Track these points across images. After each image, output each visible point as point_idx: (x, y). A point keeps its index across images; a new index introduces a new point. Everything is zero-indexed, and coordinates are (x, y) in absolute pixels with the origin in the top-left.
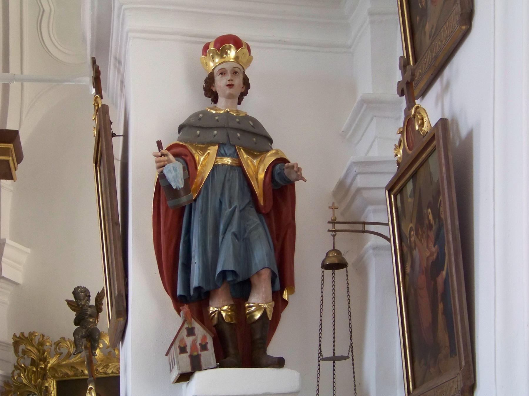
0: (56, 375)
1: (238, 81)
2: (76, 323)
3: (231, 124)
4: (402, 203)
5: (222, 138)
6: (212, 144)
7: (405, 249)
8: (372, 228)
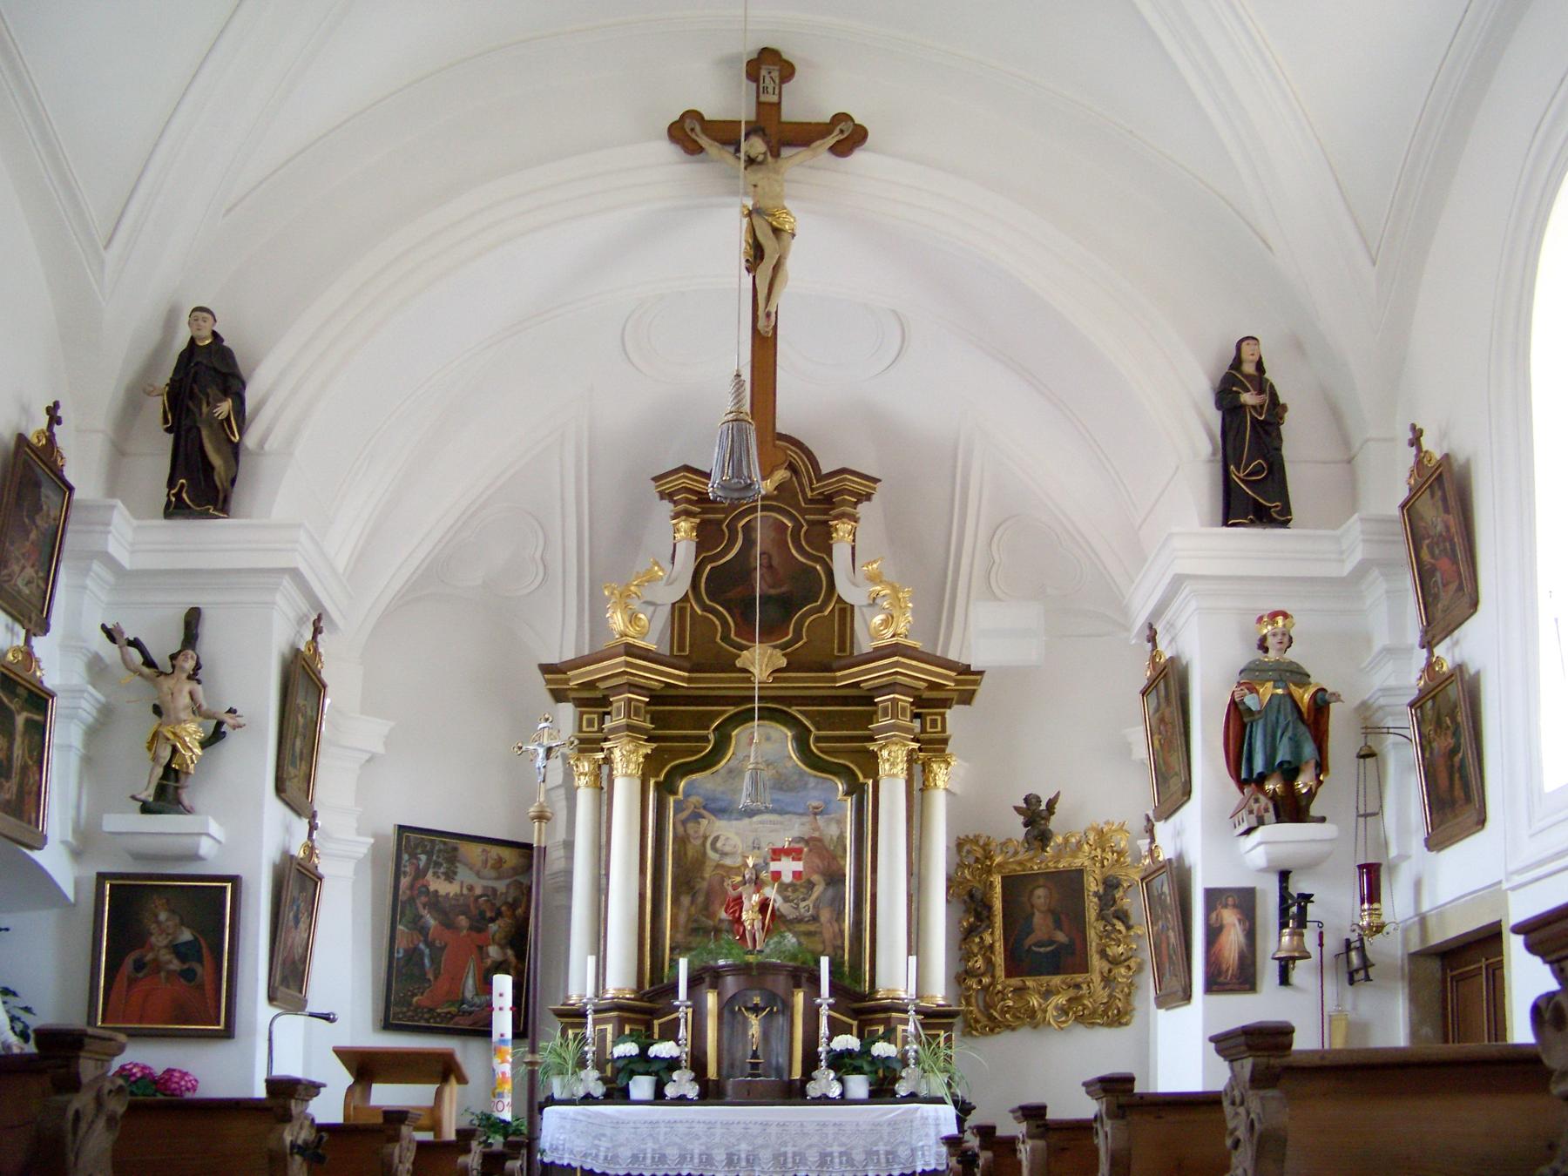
1: (1286, 640)
2: (1026, 825)
3: (1282, 668)
4: (1422, 715)
5: (1277, 677)
6: (1268, 681)
7: (1424, 743)
8: (1391, 731)
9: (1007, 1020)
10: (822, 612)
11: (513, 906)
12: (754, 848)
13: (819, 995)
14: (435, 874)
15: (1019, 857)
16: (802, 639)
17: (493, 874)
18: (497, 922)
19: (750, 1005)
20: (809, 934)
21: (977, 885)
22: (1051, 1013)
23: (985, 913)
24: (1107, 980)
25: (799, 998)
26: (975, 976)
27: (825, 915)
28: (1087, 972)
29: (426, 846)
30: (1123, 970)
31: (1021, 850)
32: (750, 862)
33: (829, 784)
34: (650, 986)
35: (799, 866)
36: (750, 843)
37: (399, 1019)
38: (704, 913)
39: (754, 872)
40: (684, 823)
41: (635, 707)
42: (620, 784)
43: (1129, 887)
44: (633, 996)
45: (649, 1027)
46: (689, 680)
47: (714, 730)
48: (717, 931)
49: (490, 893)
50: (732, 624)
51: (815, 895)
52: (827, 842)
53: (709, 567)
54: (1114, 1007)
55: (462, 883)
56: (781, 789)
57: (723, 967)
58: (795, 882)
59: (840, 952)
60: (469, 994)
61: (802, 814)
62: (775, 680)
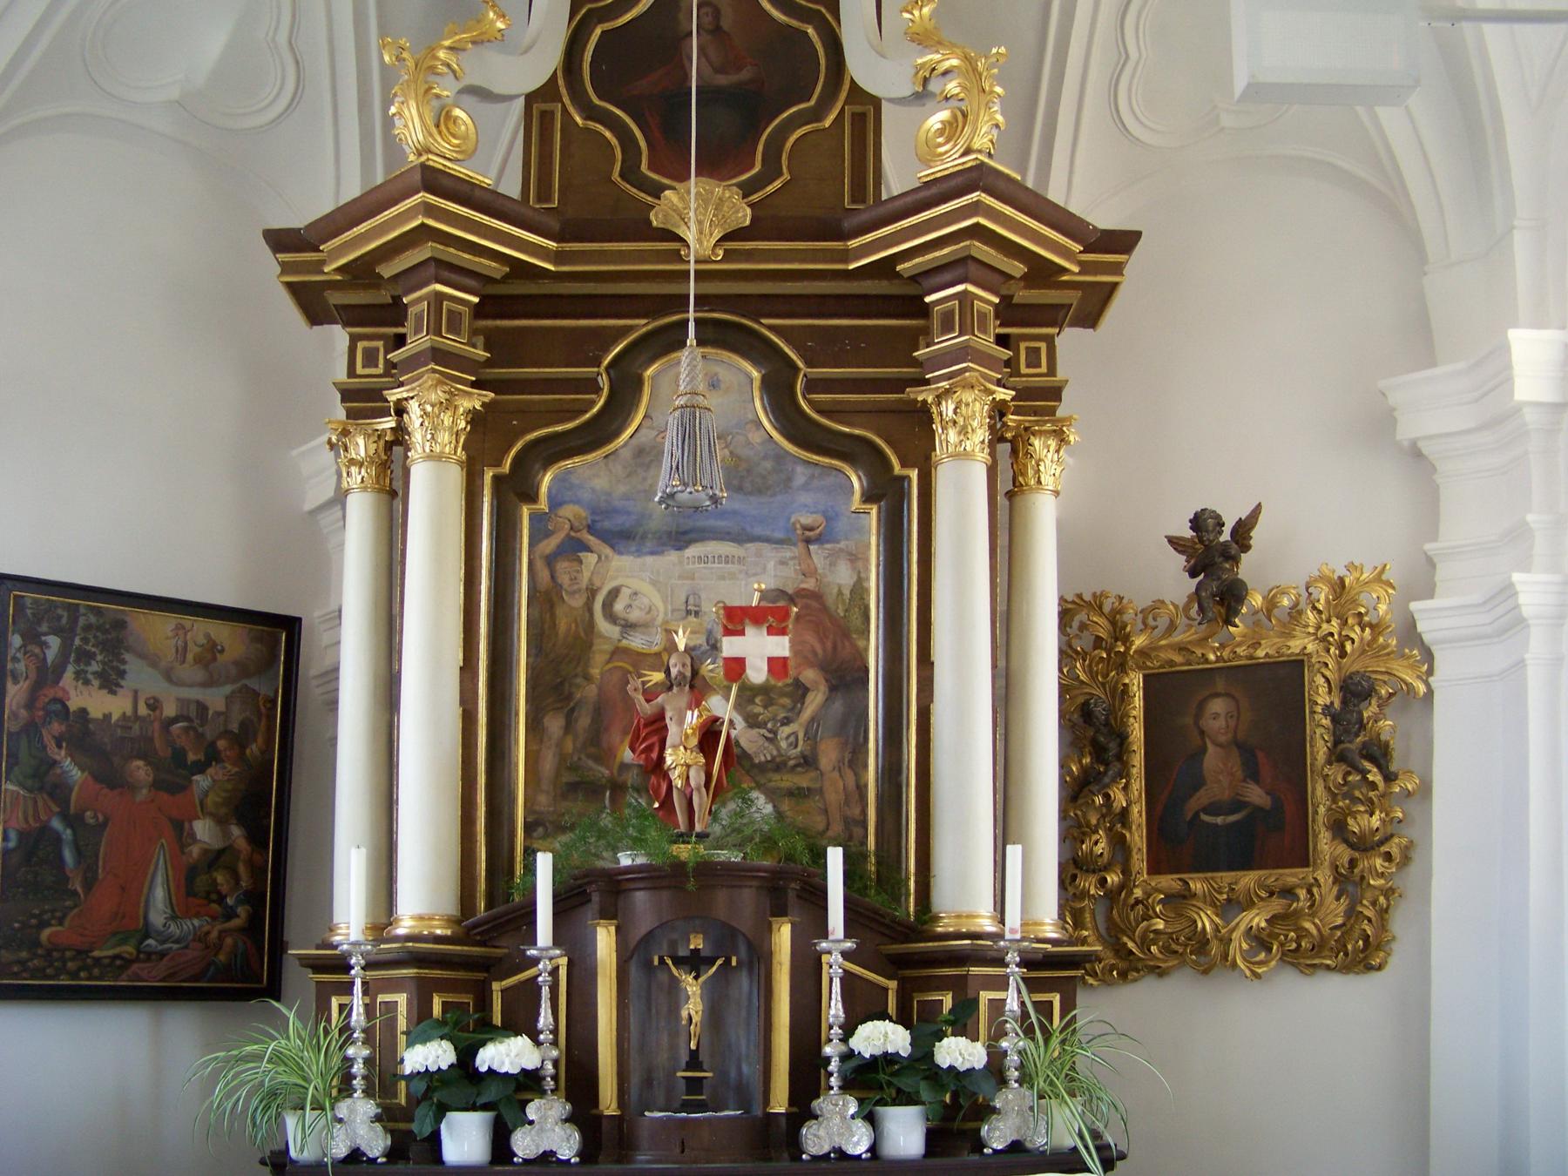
9: (1154, 957)
10: (819, 119)
11: (240, 740)
12: (688, 612)
13: (824, 934)
14: (79, 675)
15: (1177, 638)
16: (781, 174)
17: (199, 675)
18: (211, 771)
19: (682, 952)
20: (797, 794)
21: (1098, 692)
22: (1239, 944)
23: (1113, 746)
24: (1348, 881)
25: (783, 936)
26: (1094, 872)
27: (829, 755)
28: (1307, 865)
29: (60, 618)
30: (1379, 863)
31: (1181, 621)
32: (681, 642)
33: (831, 480)
34: (489, 906)
35: (780, 646)
37: (16, 976)
38: (592, 750)
39: (688, 662)
40: (550, 561)
41: (450, 311)
42: (420, 476)
43: (1391, 695)
44: (449, 932)
45: (484, 1003)
46: (558, 258)
47: (608, 369)
48: (618, 788)
49: (193, 714)
50: (643, 144)
51: (807, 713)
52: (830, 600)
53: (598, 31)
54: (1356, 935)
55: (136, 692)
57: (628, 870)
58: (773, 682)
59: (857, 831)
60: (157, 918)
61: (781, 542)
62: (729, 256)
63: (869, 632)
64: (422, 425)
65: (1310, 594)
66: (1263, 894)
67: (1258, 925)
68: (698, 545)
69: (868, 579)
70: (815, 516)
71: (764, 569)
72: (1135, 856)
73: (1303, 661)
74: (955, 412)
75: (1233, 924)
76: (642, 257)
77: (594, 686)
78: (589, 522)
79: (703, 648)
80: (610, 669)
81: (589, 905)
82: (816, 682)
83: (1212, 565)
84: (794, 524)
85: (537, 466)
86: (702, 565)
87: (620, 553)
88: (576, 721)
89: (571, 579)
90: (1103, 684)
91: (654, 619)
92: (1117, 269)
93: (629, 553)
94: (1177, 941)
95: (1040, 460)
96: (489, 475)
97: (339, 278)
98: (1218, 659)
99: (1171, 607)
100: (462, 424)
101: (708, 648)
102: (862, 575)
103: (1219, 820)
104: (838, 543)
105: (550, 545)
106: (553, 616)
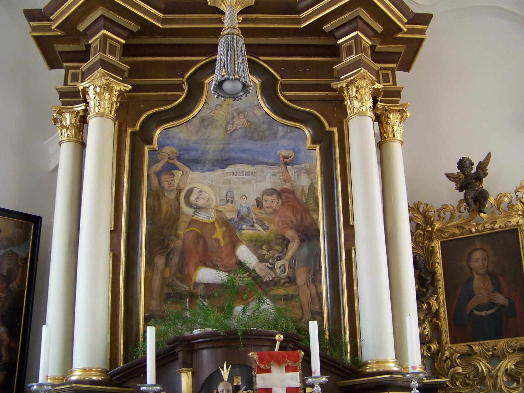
0: (443, 236)
12: (228, 201)
20: (286, 298)
22: (502, 378)
27: (302, 276)
33: (296, 133)
34: (123, 364)
36: (223, 196)
38: (179, 275)
40: (158, 174)
42: (93, 123)
44: (100, 378)
46: (164, 21)
47: (187, 80)
48: (193, 296)
51: (290, 253)
52: (298, 194)
56: (251, 138)
57: (198, 337)
61: (272, 164)
63: (318, 210)
64: (94, 98)
65: (517, 196)
66: (511, 351)
67: (510, 368)
68: (232, 166)
69: (316, 183)
70: (288, 151)
71: (265, 177)
72: (444, 335)
73: (517, 229)
74: (356, 92)
75: (498, 367)
76: (203, 21)
77: (180, 240)
78: (178, 155)
79: (235, 220)
80: (189, 231)
81: (177, 361)
82: (293, 237)
83: (471, 183)
84: (279, 155)
85: (153, 126)
86: (234, 176)
87: (193, 171)
88: (171, 260)
89: (169, 184)
90: (422, 247)
91: (210, 205)
92: (423, 32)
93: (196, 170)
94: (469, 378)
95: (394, 125)
96: (129, 130)
97: (59, 34)
98: (477, 231)
99: (451, 207)
100: (115, 99)
101: (238, 219)
102: (314, 181)
103: (483, 313)
104: (301, 165)
105: (158, 167)
106: (160, 204)
